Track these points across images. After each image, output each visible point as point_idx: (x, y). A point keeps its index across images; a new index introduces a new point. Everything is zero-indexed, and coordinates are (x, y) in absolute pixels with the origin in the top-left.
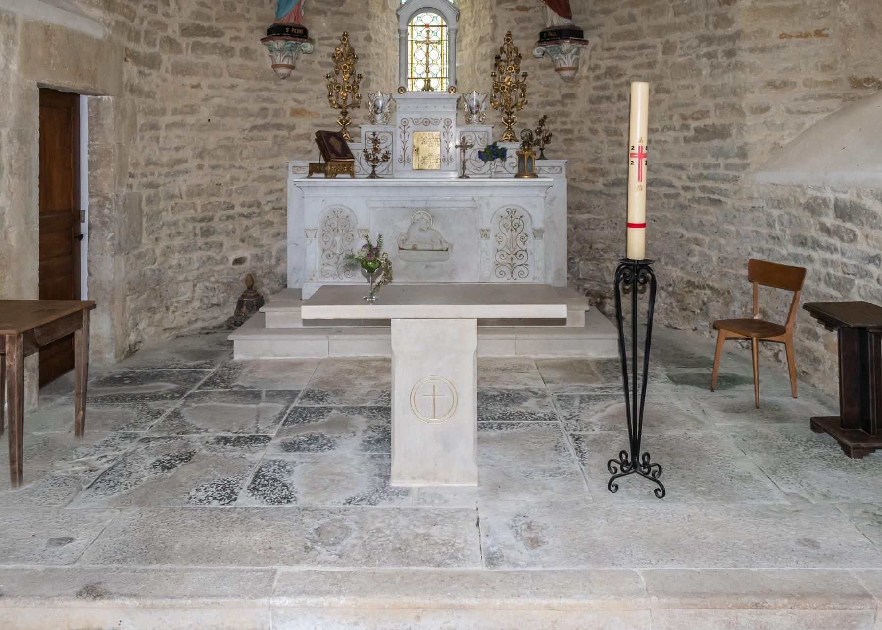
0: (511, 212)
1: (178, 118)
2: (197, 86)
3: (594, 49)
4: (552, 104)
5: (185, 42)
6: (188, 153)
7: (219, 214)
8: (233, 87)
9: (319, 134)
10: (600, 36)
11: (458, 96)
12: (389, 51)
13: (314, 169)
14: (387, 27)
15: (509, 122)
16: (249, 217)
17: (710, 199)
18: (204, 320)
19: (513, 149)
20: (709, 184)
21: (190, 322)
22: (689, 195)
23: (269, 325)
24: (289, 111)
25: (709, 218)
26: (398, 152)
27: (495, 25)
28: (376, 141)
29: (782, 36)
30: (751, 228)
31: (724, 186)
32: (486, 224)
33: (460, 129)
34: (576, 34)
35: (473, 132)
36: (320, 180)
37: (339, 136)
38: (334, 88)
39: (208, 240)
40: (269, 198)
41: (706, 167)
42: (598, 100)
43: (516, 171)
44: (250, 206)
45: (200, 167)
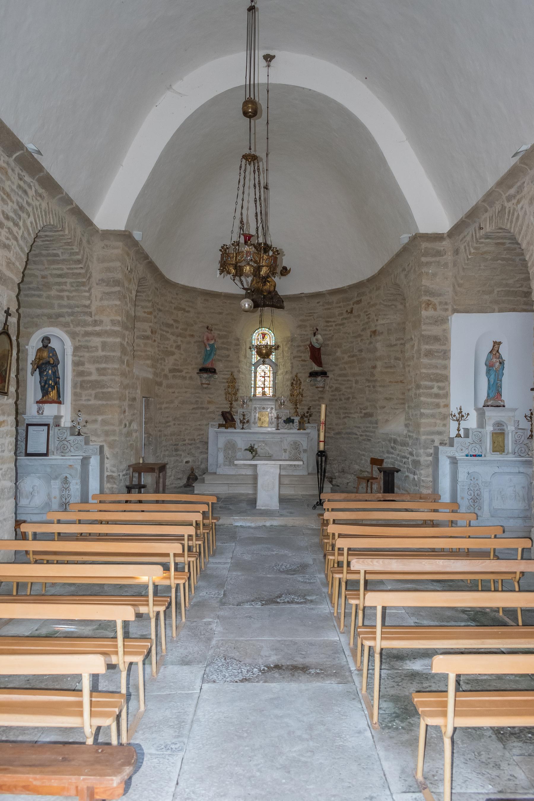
0: (295, 443)
1: (167, 405)
2: (174, 393)
3: (331, 379)
4: (315, 401)
5: (170, 375)
6: (170, 419)
7: (181, 443)
8: (186, 392)
9: (223, 412)
10: (334, 374)
11: (276, 398)
12: (247, 376)
13: (220, 426)
14: (246, 365)
15: (296, 408)
16: (191, 445)
17: (368, 439)
18: (175, 484)
19: (297, 419)
20: (368, 434)
21: (171, 484)
22: (362, 438)
23: (195, 492)
24: (206, 402)
25: (367, 446)
26: (252, 420)
27: (292, 367)
28: (244, 415)
29: (390, 382)
30: (378, 449)
31: (371, 434)
32: (286, 447)
33: (277, 411)
34: (324, 374)
35: (282, 412)
36: (223, 429)
37: (230, 413)
38: (227, 393)
39: (177, 453)
40: (199, 437)
41: (367, 427)
42: (332, 400)
43: (298, 428)
44: (192, 440)
45: (174, 424)
